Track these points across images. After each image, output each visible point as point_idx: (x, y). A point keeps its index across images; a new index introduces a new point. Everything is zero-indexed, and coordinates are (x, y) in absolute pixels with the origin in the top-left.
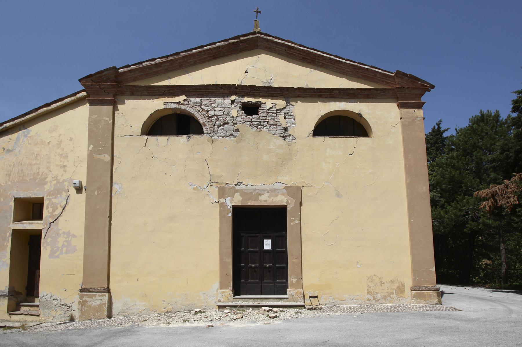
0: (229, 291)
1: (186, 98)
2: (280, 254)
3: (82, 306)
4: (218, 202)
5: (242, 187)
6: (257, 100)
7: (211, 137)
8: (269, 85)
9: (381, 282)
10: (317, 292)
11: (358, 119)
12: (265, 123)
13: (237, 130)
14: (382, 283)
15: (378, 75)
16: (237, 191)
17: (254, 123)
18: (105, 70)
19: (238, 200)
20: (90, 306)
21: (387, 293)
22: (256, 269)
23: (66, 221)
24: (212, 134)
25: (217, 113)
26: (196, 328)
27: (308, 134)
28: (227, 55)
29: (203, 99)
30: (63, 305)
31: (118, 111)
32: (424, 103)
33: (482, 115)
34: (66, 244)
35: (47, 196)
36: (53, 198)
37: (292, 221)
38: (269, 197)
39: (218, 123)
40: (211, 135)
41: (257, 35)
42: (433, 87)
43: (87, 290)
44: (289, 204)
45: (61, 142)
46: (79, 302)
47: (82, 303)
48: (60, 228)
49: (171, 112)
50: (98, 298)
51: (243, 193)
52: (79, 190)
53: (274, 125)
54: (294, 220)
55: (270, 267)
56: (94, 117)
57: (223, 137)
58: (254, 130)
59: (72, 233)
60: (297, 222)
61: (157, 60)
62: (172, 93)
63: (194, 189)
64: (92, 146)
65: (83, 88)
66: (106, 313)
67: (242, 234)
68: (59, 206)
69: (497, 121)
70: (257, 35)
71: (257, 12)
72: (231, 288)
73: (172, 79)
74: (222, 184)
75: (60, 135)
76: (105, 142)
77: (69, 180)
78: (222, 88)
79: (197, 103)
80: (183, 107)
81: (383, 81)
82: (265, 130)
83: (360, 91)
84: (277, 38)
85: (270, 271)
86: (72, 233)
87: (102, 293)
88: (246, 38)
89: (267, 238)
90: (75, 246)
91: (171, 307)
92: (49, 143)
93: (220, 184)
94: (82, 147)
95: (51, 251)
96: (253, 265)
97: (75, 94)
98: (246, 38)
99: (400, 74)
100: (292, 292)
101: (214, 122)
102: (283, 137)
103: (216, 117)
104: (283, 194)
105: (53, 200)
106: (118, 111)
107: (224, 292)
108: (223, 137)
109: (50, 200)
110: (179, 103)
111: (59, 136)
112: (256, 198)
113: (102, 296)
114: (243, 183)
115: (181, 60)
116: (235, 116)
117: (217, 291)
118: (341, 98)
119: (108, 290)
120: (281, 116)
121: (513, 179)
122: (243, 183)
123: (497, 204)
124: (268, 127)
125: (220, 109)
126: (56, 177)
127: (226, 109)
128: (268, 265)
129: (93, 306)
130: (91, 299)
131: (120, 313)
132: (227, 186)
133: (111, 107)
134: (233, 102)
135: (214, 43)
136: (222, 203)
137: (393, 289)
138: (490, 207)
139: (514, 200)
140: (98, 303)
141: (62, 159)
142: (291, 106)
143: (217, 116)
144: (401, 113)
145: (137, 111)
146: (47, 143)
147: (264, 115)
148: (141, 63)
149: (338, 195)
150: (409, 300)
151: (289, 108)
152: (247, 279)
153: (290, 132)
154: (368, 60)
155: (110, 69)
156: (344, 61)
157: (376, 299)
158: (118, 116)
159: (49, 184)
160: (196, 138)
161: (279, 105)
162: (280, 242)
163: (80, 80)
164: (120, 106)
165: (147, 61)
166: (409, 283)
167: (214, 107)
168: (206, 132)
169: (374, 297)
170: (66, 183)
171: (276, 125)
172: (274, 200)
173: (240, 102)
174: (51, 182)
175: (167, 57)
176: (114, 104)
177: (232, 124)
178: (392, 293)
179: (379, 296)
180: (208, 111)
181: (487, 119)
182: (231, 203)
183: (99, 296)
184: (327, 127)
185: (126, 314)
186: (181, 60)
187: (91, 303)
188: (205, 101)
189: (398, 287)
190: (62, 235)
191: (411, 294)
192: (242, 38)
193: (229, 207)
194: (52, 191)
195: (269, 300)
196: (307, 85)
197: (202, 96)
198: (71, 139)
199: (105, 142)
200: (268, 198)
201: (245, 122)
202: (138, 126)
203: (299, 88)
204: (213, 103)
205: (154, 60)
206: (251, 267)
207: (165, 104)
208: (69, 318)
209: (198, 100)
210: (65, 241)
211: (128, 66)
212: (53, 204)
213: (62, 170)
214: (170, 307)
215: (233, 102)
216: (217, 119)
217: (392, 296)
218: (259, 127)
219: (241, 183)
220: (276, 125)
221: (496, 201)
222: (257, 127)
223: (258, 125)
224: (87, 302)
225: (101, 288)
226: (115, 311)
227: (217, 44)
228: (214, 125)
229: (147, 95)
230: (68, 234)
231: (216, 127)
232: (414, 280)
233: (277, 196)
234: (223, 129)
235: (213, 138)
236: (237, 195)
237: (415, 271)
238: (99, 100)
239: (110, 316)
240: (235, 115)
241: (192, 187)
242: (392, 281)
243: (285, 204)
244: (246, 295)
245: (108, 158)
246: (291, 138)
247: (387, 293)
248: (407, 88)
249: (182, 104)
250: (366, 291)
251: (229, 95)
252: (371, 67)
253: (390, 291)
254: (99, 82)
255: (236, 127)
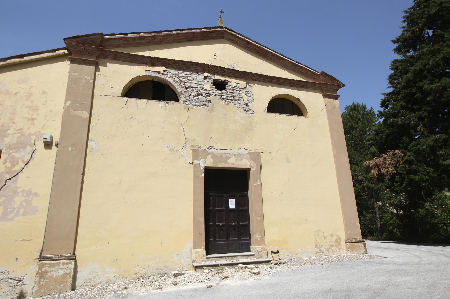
0: (203, 251)
1: (165, 69)
2: (243, 212)
3: (41, 277)
4: (193, 163)
5: (213, 150)
6: (227, 79)
7: (187, 104)
8: (233, 68)
9: (324, 236)
10: (277, 247)
11: (296, 102)
12: (232, 98)
13: (210, 101)
14: (325, 237)
15: (309, 72)
16: (209, 154)
17: (223, 97)
18: (93, 35)
19: (210, 163)
20: (51, 277)
21: (329, 245)
22: (223, 228)
23: (28, 178)
24: (188, 102)
25: (192, 85)
26: (195, 290)
27: (263, 110)
28: (200, 40)
29: (181, 72)
30: (11, 279)
31: (100, 71)
32: (339, 96)
33: (355, 106)
34: (24, 204)
35: (6, 150)
36: (14, 152)
37: (255, 182)
38: (236, 160)
39: (193, 94)
40: (187, 103)
41: (224, 29)
42: (344, 85)
43: (49, 257)
44: (252, 167)
45: (31, 94)
46: (38, 274)
47: (41, 275)
48: (18, 185)
49: (150, 79)
50: (62, 266)
51: (214, 156)
52: (48, 145)
53: (238, 100)
54: (257, 181)
55: (223, 226)
56: (74, 74)
57: (197, 106)
58: (224, 103)
59: (34, 191)
60: (259, 183)
61: (141, 34)
62: (153, 63)
63: (171, 150)
64: (70, 102)
65: (65, 46)
66: (70, 285)
67: (210, 194)
68: (20, 161)
69: (365, 110)
70: (224, 29)
71: (222, 12)
72: (204, 247)
73: (152, 51)
74: (196, 147)
75: (32, 87)
76: (82, 100)
77: (37, 134)
78: (197, 65)
79: (175, 75)
80: (163, 77)
81: (312, 77)
82: (232, 103)
83: (298, 82)
84: (239, 34)
85: (235, 229)
86: (34, 191)
87: (68, 261)
88: (216, 30)
89: (232, 198)
90: (37, 206)
91: (143, 272)
92: (16, 94)
93: (194, 147)
94: (58, 101)
95: (3, 212)
96: (221, 224)
97: (55, 51)
98: (216, 30)
99: (324, 74)
100: (257, 249)
101: (190, 93)
102: (245, 110)
103: (192, 89)
104: (247, 159)
105: (13, 154)
106: (100, 71)
107: (198, 252)
108: (197, 106)
109: (9, 154)
110: (159, 72)
111: (30, 88)
112: (226, 161)
113: (67, 264)
114: (214, 147)
115: (162, 38)
116: (208, 89)
117: (191, 251)
118: (285, 85)
119: (74, 257)
120: (243, 93)
121: (388, 154)
122: (214, 147)
123: (381, 172)
124: (234, 101)
125: (195, 82)
126: (21, 129)
127: (200, 83)
128: (233, 224)
129: (54, 277)
130: (53, 269)
131: (86, 283)
132: (200, 149)
133: (94, 67)
134: (206, 78)
135: (191, 29)
136: (196, 164)
137: (333, 242)
138: (377, 174)
139: (391, 170)
140: (62, 272)
141: (30, 111)
142: (249, 87)
143: (192, 87)
144: (325, 101)
145: (118, 75)
146: (14, 93)
147: (231, 91)
148: (126, 34)
149: (288, 161)
150: (345, 251)
151: (249, 88)
152: (215, 237)
153: (250, 107)
154: (304, 60)
155: (98, 34)
156: (286, 59)
157: (322, 251)
158: (99, 76)
159: (11, 136)
160: (173, 104)
161: (242, 85)
162: (243, 201)
163: (65, 39)
164: (101, 68)
165: (132, 33)
166: (343, 237)
167: (190, 80)
168: (183, 100)
169: (320, 249)
170: (33, 137)
171: (240, 100)
172: (240, 164)
173: (212, 78)
174: (13, 135)
175: (151, 33)
176: (97, 65)
177: (206, 96)
178: (333, 246)
179: (323, 249)
180: (185, 83)
181: (358, 109)
182: (204, 164)
183: (64, 264)
184: (279, 106)
185: (93, 284)
186: (162, 38)
187: (53, 273)
188: (182, 74)
189: (337, 240)
190: (21, 193)
191: (346, 246)
192: (213, 30)
193: (202, 169)
194: (14, 144)
195: (239, 257)
196: (261, 72)
197: (180, 69)
198: (44, 93)
199: (82, 100)
200: (235, 162)
201: (216, 95)
202: (120, 88)
203: (256, 74)
204: (189, 77)
205: (139, 33)
206: (219, 226)
207: (146, 71)
208: (18, 295)
209: (176, 72)
210: (25, 201)
211: (115, 35)
212: (13, 158)
213: (30, 122)
214: (142, 272)
215: (206, 78)
216: (193, 90)
217: (333, 248)
218: (227, 100)
219: (212, 147)
220: (240, 100)
221: (380, 170)
222: (226, 101)
223: (227, 99)
224: (48, 272)
225: (66, 254)
226: (79, 281)
227: (194, 31)
228: (190, 95)
229: (129, 62)
230: (29, 193)
231: (192, 97)
232: (347, 234)
233: (242, 159)
234: (198, 99)
235: (189, 106)
236: (209, 157)
237: (347, 225)
238: (82, 60)
239: (73, 289)
240: (208, 89)
241: (169, 148)
242: (332, 235)
243: (249, 167)
244: (240, 252)
245: (86, 115)
246: (250, 112)
247: (329, 245)
248: (329, 84)
249: (162, 74)
250: (314, 245)
251: (203, 71)
252: (305, 66)
253: (331, 243)
254: (84, 44)
255: (209, 98)
